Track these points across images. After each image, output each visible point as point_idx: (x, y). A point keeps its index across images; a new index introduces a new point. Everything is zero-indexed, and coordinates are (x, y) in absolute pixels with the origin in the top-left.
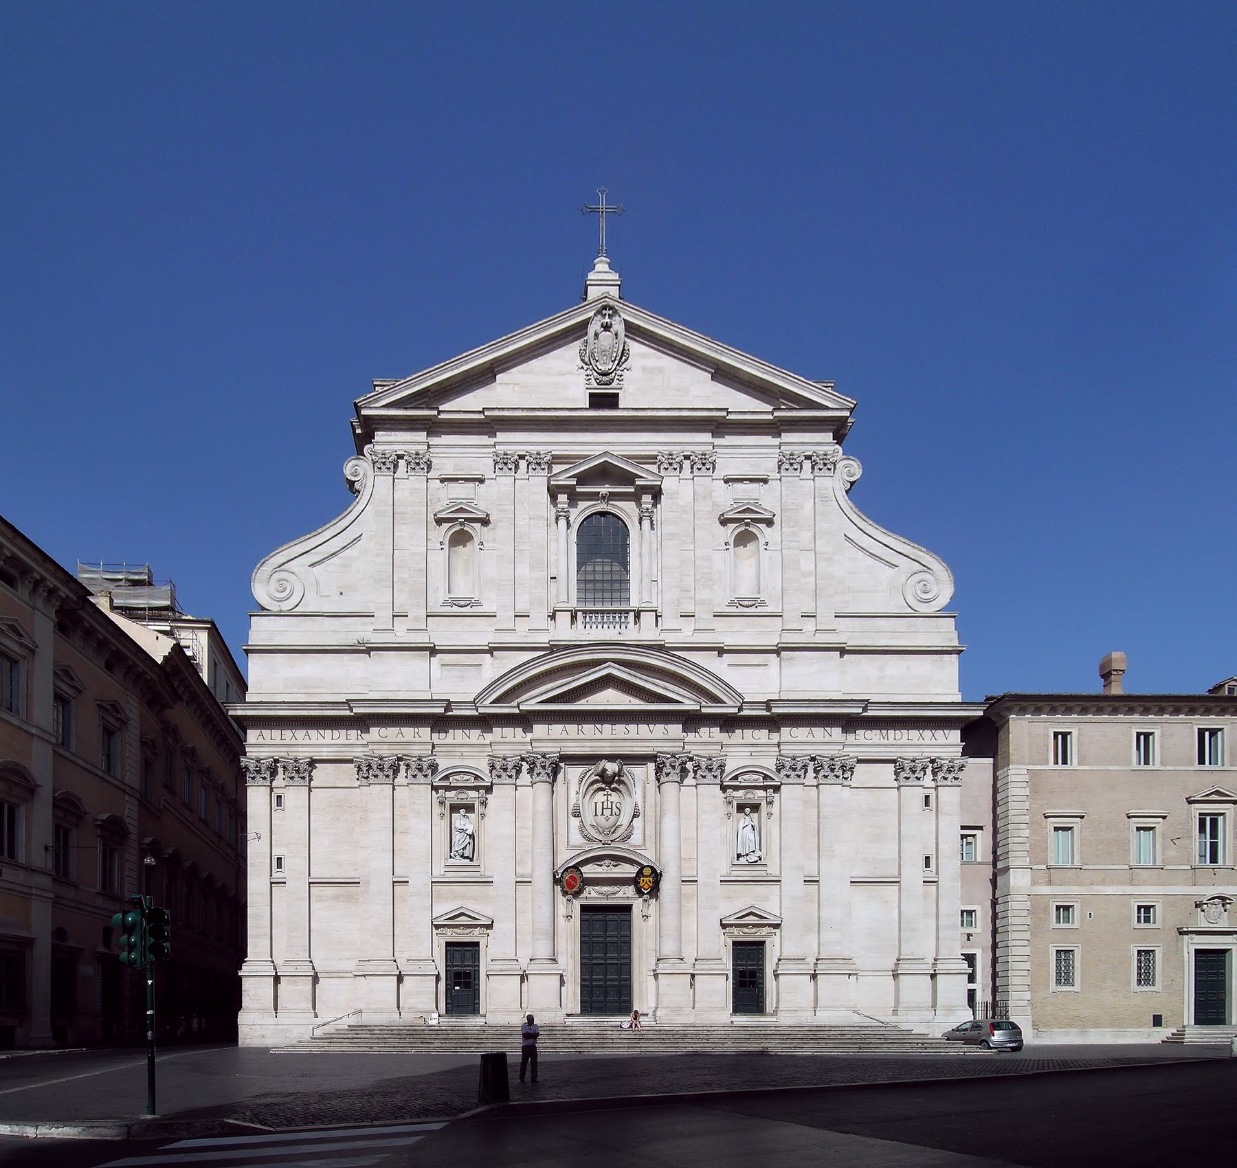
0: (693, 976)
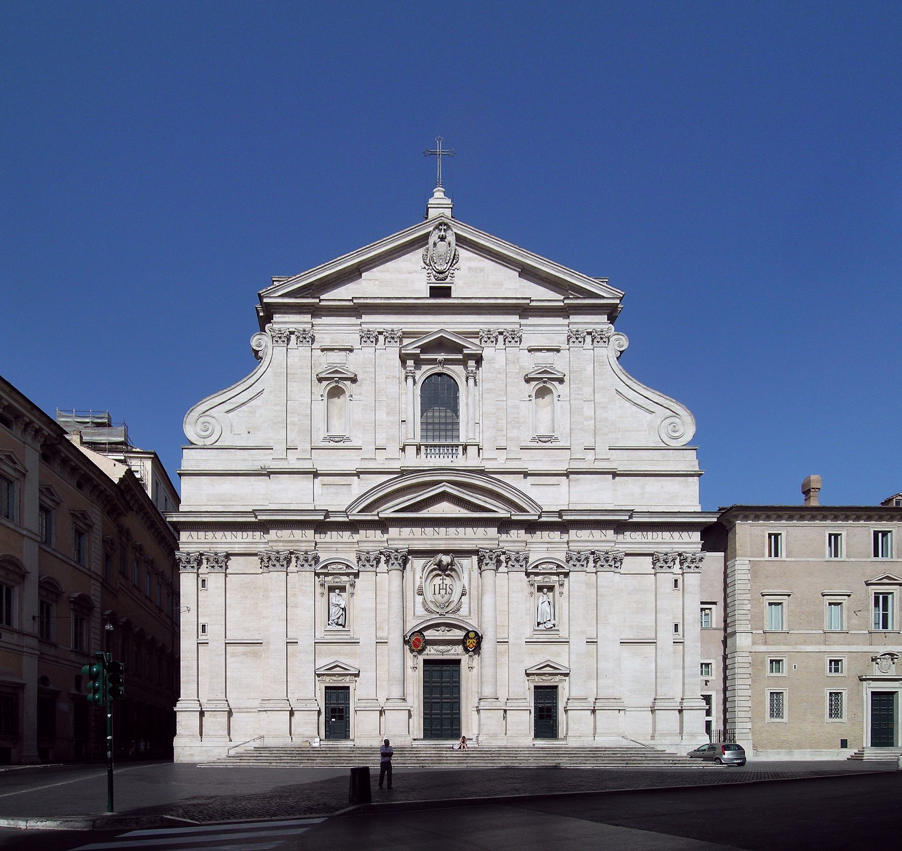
0: (505, 711)
